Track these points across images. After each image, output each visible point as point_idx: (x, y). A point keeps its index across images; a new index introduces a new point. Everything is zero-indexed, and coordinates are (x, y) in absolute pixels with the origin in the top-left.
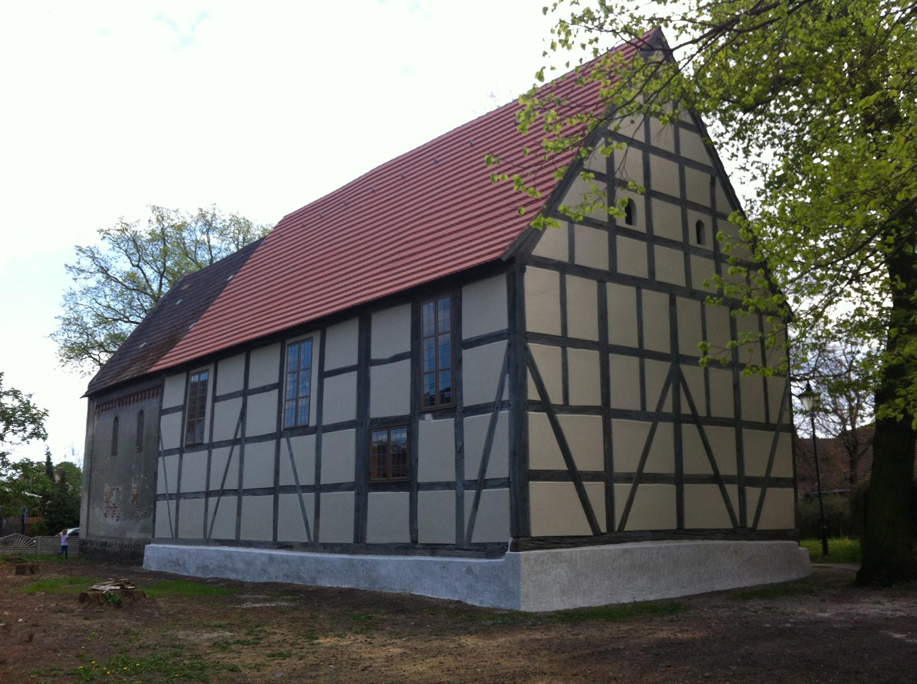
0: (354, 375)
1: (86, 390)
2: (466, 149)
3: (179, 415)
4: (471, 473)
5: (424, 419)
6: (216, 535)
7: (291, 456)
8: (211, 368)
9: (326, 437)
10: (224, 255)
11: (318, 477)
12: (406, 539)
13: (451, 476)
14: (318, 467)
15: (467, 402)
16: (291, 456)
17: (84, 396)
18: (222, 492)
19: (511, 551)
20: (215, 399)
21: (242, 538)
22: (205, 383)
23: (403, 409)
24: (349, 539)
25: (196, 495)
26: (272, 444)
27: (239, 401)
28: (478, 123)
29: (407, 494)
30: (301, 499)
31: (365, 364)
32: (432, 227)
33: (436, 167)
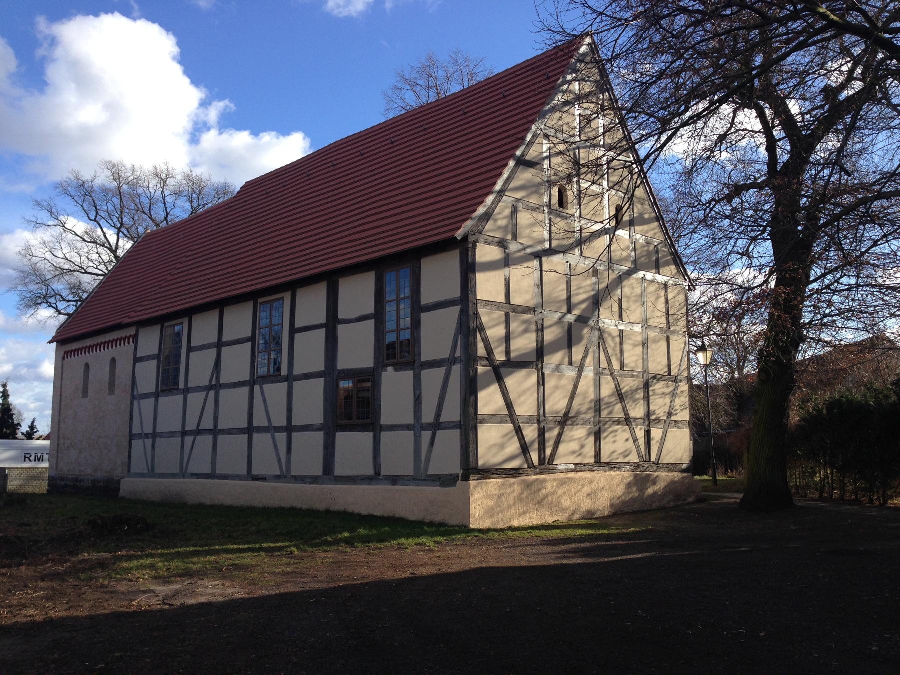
0: (322, 332)
1: (54, 334)
2: (387, 145)
3: (154, 363)
4: (191, 426)
5: (386, 371)
6: (193, 468)
7: (265, 401)
8: (186, 321)
9: (297, 385)
10: (173, 223)
11: (289, 419)
12: (370, 472)
13: (410, 420)
14: (290, 410)
15: (424, 358)
16: (265, 401)
17: (50, 342)
18: (198, 432)
19: (462, 481)
20: (190, 349)
21: (218, 472)
22: (179, 335)
23: (368, 362)
24: (319, 472)
25: (172, 434)
26: (246, 390)
27: (213, 352)
28: (341, 145)
29: (371, 434)
30: (274, 438)
31: (332, 323)
32: (391, 203)
33: (362, 160)
